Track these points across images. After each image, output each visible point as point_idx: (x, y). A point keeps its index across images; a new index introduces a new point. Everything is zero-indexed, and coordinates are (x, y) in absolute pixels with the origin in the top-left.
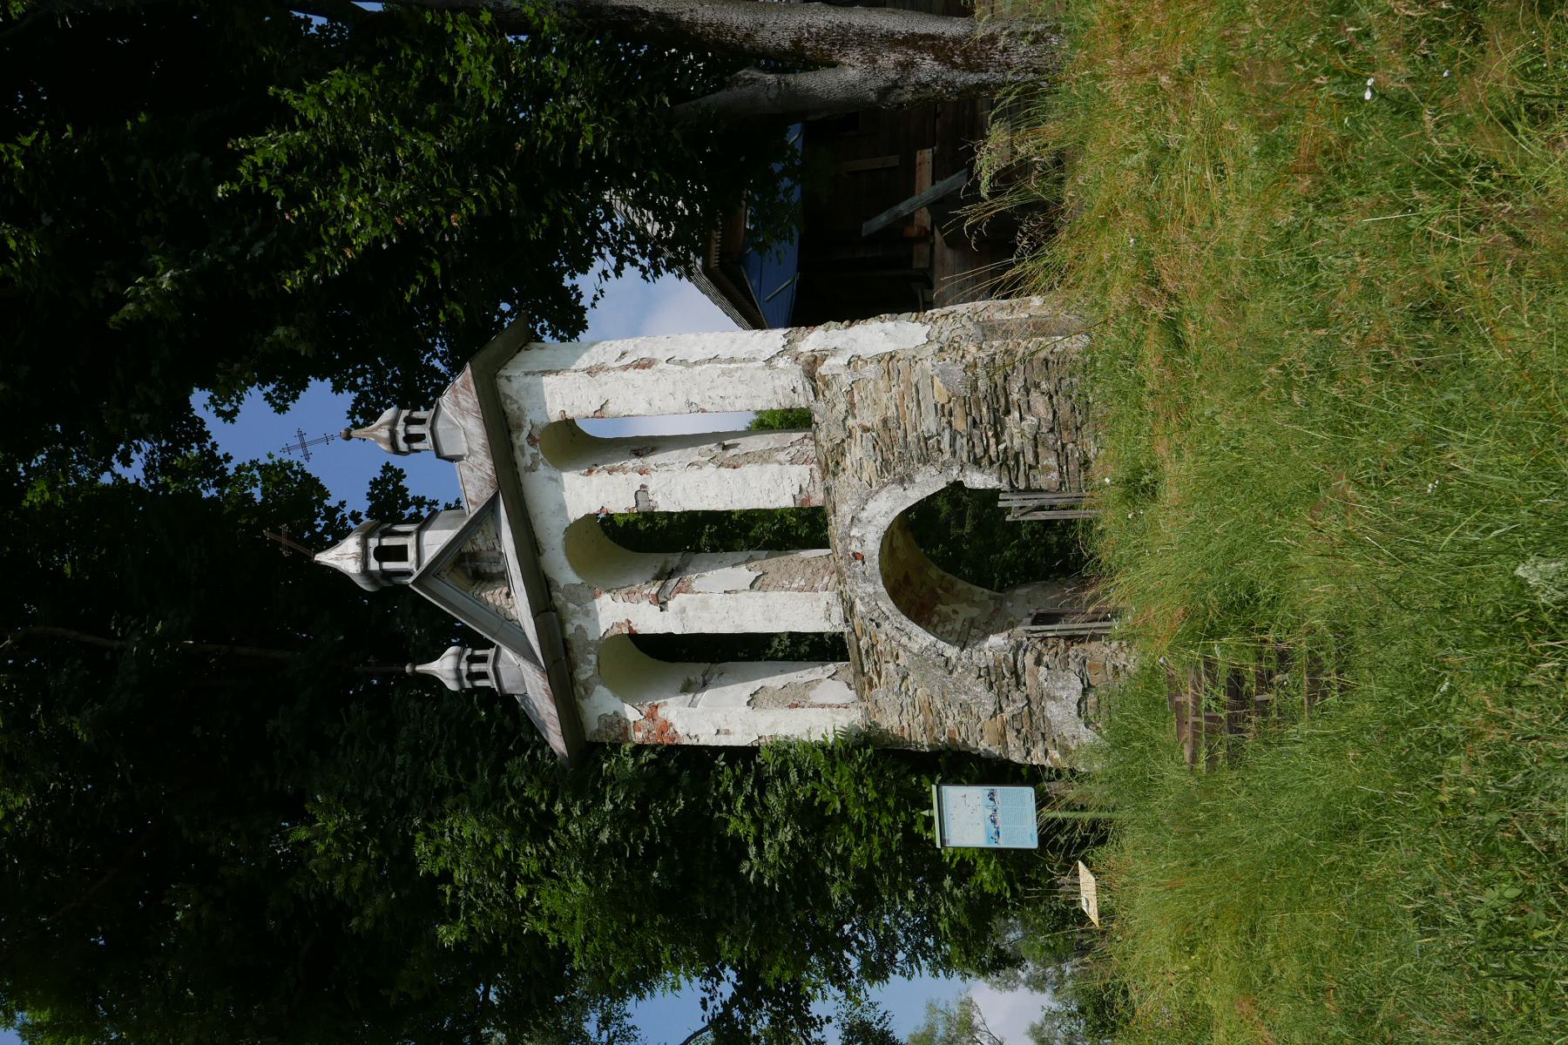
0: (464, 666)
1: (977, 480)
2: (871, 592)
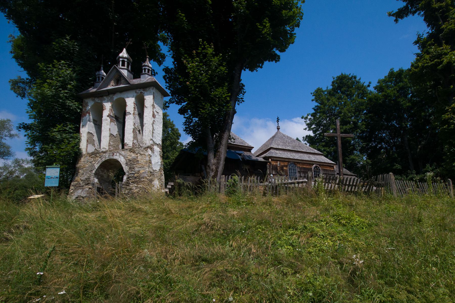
1: (125, 178)
2: (107, 157)
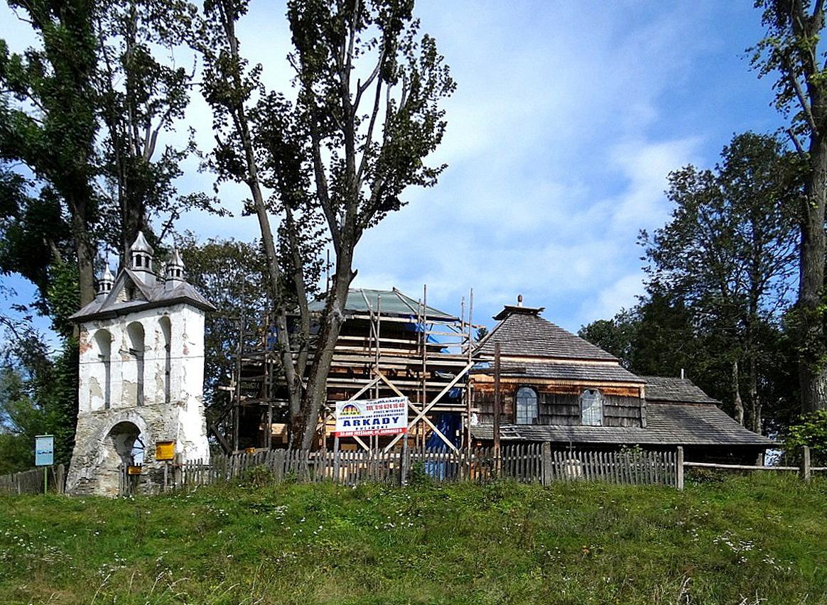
0: (106, 282)
